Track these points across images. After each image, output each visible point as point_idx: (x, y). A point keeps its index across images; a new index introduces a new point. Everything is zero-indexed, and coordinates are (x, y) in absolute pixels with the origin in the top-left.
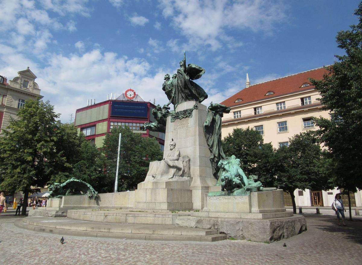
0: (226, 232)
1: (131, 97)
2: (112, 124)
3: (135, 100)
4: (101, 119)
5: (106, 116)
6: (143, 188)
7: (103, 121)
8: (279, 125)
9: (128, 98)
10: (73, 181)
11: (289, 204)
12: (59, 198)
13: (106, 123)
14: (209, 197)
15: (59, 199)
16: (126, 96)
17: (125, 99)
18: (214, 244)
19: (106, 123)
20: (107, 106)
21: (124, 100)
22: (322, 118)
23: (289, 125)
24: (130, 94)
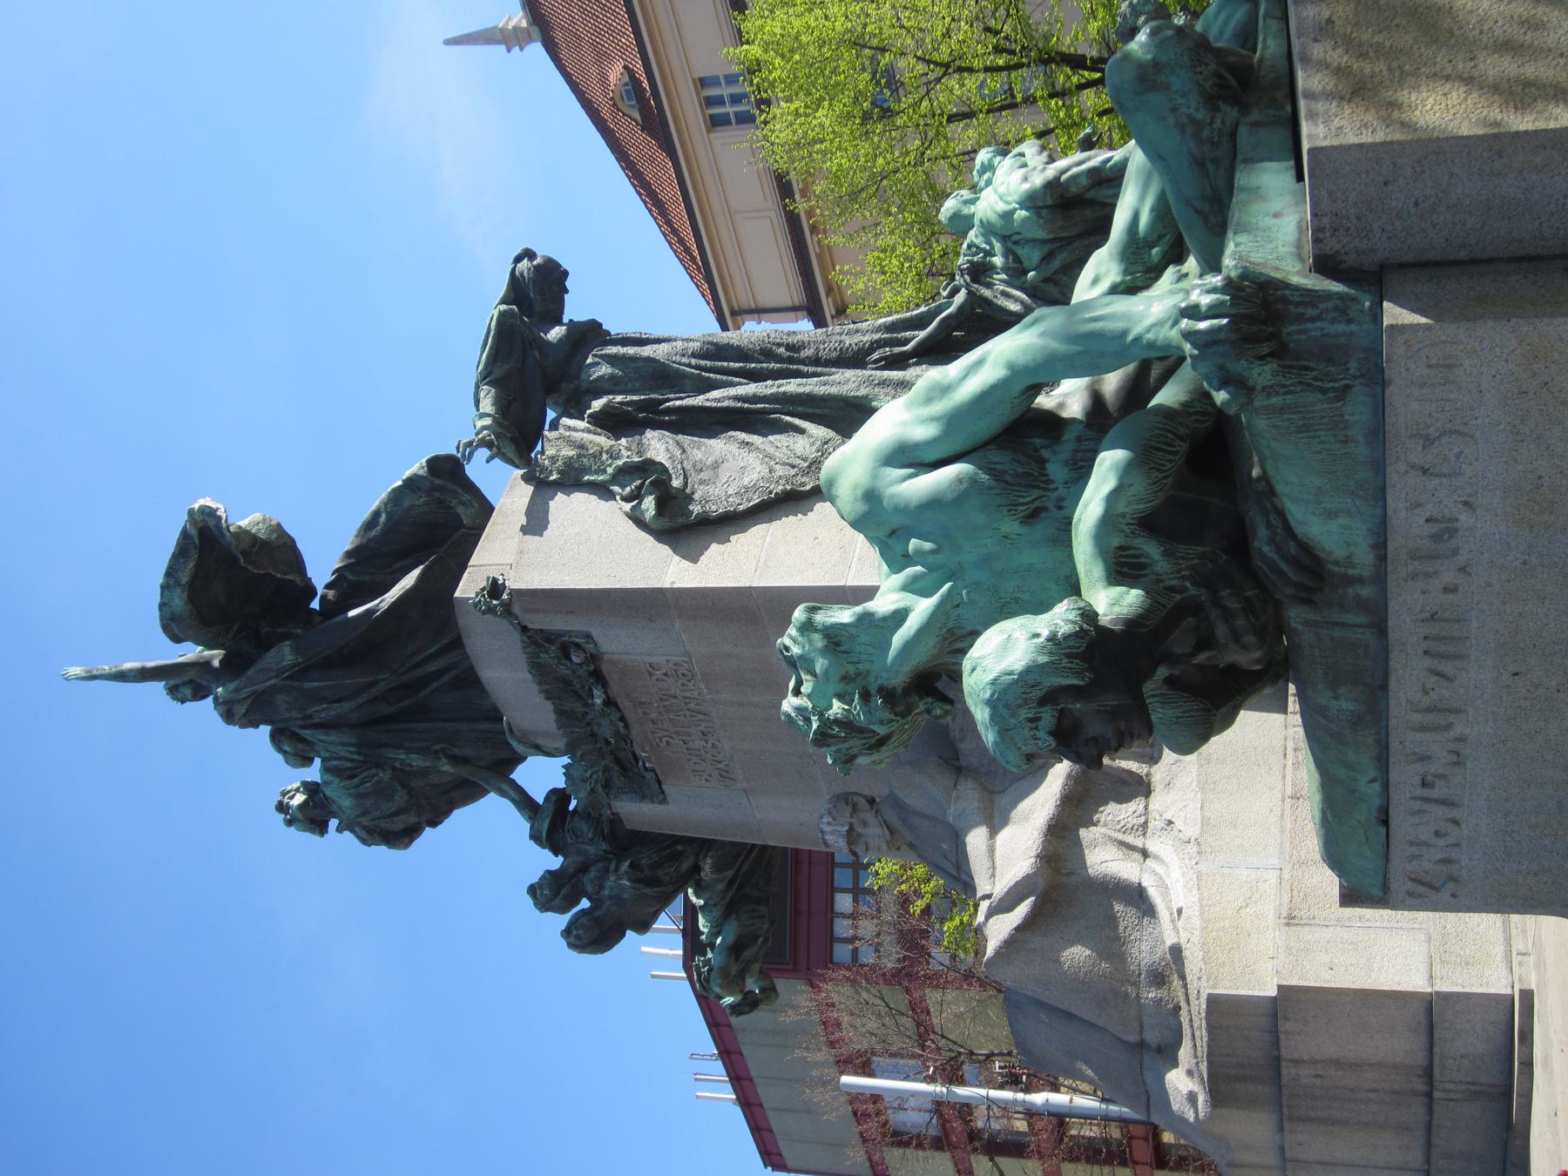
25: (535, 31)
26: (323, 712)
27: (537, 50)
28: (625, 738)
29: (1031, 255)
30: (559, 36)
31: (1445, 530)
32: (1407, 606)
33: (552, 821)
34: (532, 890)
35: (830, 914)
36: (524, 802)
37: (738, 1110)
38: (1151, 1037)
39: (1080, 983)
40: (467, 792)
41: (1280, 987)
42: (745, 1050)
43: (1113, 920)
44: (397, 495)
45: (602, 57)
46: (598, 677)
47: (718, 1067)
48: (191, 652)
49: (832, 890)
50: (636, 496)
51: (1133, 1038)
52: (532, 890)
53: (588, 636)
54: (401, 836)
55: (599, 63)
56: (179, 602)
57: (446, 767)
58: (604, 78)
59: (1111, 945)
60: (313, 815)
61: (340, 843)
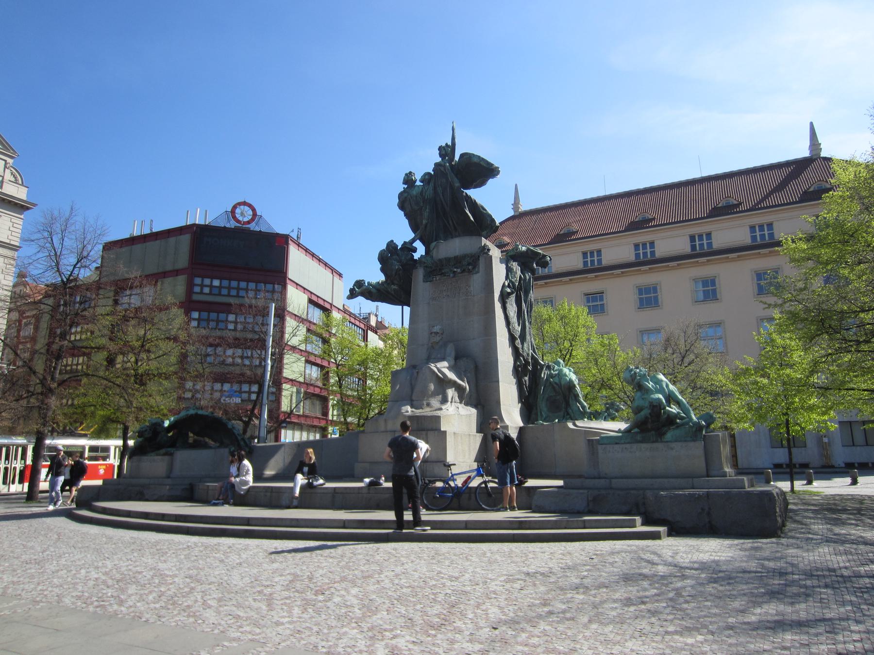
0: (670, 518)
1: (246, 219)
2: (198, 281)
3: (253, 227)
4: (169, 268)
5: (183, 261)
6: (383, 429)
7: (176, 273)
8: (656, 298)
9: (238, 221)
10: (196, 414)
11: (51, 508)
12: (165, 454)
13: (182, 280)
14: (604, 446)
15: (166, 458)
16: (234, 217)
17: (232, 224)
18: (608, 549)
19: (182, 280)
20: (186, 239)
21: (228, 226)
22: (393, 258)
23: (664, 296)
24: (243, 215)
25: (517, 214)
26: (440, 190)
27: (512, 213)
28: (443, 274)
29: (557, 380)
30: (516, 221)
31: (672, 449)
32: (659, 445)
33: (408, 248)
34: (392, 241)
35: (212, 278)
36: (413, 240)
37: (127, 236)
38: (415, 403)
39: (426, 387)
40: (414, 227)
41: (445, 432)
42: (158, 242)
43: (438, 395)
44: (490, 216)
45: (511, 235)
46: (463, 271)
47: (147, 231)
48: (457, 158)
49: (221, 279)
50: (509, 286)
51: (414, 398)
52: (392, 241)
53: (478, 272)
54: (402, 206)
55: (509, 234)
56: (475, 160)
57: (424, 222)
58: (505, 235)
59: (434, 394)
60: (409, 180)
61: (401, 187)
